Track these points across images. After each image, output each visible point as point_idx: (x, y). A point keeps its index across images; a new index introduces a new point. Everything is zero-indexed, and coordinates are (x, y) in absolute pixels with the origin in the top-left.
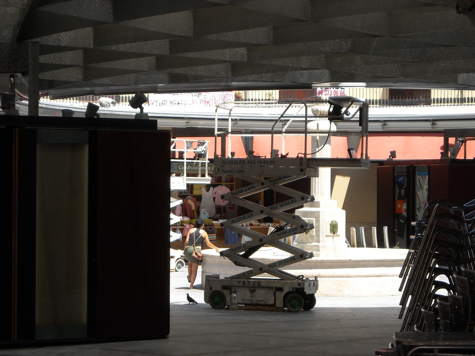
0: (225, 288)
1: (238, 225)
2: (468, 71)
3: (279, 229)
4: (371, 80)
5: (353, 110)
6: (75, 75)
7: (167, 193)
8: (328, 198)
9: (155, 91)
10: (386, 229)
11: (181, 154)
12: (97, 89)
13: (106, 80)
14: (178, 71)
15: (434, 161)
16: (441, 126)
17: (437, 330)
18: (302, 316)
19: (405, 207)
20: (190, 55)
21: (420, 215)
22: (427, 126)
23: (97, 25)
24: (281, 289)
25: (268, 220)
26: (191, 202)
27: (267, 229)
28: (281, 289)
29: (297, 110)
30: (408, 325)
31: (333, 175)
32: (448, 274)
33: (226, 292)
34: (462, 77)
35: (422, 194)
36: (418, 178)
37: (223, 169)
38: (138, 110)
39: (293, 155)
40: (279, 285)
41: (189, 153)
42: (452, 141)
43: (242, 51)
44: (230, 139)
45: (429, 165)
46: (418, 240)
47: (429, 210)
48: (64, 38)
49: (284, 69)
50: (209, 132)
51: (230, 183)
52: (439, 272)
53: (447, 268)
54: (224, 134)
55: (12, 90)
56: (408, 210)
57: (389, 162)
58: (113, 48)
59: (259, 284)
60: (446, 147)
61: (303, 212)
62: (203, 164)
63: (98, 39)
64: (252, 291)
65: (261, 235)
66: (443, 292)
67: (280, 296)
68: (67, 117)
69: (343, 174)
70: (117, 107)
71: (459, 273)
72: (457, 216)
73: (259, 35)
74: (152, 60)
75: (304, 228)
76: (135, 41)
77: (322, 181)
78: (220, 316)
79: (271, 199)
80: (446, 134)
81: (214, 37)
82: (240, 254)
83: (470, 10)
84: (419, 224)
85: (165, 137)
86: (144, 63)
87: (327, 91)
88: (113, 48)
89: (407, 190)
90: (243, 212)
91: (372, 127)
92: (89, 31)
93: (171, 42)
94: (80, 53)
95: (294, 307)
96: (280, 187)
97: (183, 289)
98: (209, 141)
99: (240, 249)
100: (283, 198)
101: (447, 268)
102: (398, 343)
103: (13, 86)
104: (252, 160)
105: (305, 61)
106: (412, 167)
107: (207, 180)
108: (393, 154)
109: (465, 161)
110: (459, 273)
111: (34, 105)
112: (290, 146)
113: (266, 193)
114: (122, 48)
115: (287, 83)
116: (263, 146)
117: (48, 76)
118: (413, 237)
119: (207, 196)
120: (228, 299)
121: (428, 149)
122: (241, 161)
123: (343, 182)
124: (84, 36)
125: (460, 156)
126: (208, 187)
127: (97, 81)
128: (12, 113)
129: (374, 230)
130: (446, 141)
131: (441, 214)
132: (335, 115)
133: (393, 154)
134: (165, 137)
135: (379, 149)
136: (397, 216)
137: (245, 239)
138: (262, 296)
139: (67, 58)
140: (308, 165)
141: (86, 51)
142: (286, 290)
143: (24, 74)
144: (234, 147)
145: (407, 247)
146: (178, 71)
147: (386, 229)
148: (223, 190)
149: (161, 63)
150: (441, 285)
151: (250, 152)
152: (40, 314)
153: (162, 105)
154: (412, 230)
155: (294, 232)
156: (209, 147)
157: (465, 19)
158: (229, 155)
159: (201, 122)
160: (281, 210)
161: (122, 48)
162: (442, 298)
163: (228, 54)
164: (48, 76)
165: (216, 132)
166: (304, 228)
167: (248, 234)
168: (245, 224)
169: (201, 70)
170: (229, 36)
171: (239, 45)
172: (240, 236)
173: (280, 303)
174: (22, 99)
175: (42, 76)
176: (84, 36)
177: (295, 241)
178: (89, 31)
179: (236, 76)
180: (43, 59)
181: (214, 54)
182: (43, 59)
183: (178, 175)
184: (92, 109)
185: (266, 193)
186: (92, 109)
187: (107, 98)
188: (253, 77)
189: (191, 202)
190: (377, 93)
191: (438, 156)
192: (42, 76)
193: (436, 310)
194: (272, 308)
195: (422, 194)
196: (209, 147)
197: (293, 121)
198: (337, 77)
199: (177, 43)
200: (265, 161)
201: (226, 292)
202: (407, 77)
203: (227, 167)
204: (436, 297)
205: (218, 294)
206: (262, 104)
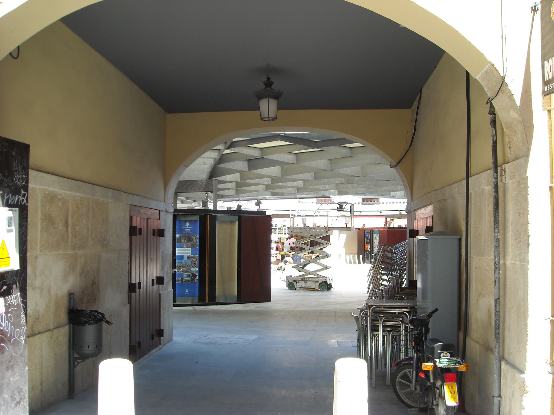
0: (294, 281)
1: (300, 255)
2: (395, 191)
3: (317, 256)
4: (356, 194)
5: (348, 207)
6: (232, 192)
7: (270, 242)
8: (338, 245)
9: (265, 199)
10: (361, 256)
11: (276, 225)
12: (241, 198)
13: (245, 195)
14: (274, 191)
15: (381, 228)
16: (384, 213)
17: (383, 298)
18: (326, 293)
19: (369, 247)
20: (280, 184)
21: (375, 250)
22: (378, 213)
23: (241, 172)
24: (318, 282)
25: (312, 252)
26: (280, 245)
27: (312, 256)
28: (318, 282)
29: (324, 206)
30: (370, 297)
31: (340, 233)
32: (387, 275)
33: (295, 283)
34: (392, 193)
35: (376, 242)
36: (374, 235)
37: (295, 233)
38: (258, 207)
39: (322, 226)
40: (317, 280)
41: (279, 225)
42: (388, 219)
43: (302, 182)
44: (296, 218)
45: (380, 231)
46: (375, 261)
47: (379, 249)
48: (228, 177)
49: (319, 190)
50: (288, 216)
51: (296, 237)
52: (383, 274)
53: (386, 272)
54: (294, 217)
55: (207, 199)
56: (370, 248)
57: (362, 228)
58: (248, 181)
59: (308, 280)
60: (386, 222)
61: (327, 250)
62: (285, 229)
63: (242, 178)
64: (306, 282)
65: (309, 259)
66: (385, 283)
67: (317, 284)
68: (229, 212)
69: (343, 233)
70: (249, 206)
71: (392, 275)
72: (391, 252)
73: (308, 176)
74: (264, 186)
75: (327, 256)
76: (257, 179)
77: (334, 236)
78: (292, 292)
79: (313, 244)
80: (386, 216)
81: (290, 177)
82: (302, 267)
83: (395, 166)
84: (375, 255)
85: (269, 218)
86: (261, 188)
87: (337, 199)
88: (248, 181)
89: (370, 240)
90: (302, 249)
91: (355, 214)
92: (238, 174)
93: (272, 179)
94: (235, 183)
95: (323, 289)
96: (317, 239)
97: (277, 282)
98: (287, 219)
99: (300, 265)
100: (318, 244)
101: (386, 272)
102: (367, 304)
103: (207, 197)
104: (306, 227)
105: (327, 187)
106: (372, 231)
107: (287, 236)
108: (364, 225)
109: (394, 228)
110: (392, 275)
111: (215, 205)
112: (322, 222)
113: (312, 241)
114: (252, 181)
115: (320, 196)
116: (310, 223)
117: (221, 193)
118: (372, 260)
119: (287, 243)
120: (295, 286)
121: (379, 223)
122: (301, 228)
123: (344, 236)
124: (236, 177)
125: (392, 226)
126: (287, 239)
127: (241, 195)
128: (207, 209)
129: (356, 256)
130: (386, 219)
131: (384, 251)
132: (340, 209)
133: (364, 225)
134: (269, 218)
135: (358, 223)
136: (365, 251)
137: (302, 261)
138: (311, 285)
139: (229, 185)
140: (329, 229)
141: (237, 183)
142: (319, 282)
143: (211, 192)
144: (298, 223)
145: (371, 264)
146: (274, 191)
147: (361, 256)
148: (293, 240)
149: (268, 187)
150: (384, 280)
151: (305, 225)
152: (218, 291)
153: (269, 206)
154: (372, 257)
155: (323, 258)
156: (287, 222)
157: (393, 170)
158: (295, 226)
159: (496, 385)
160: (317, 249)
161: (252, 181)
162: (386, 286)
163: (295, 184)
164: (221, 193)
165: (291, 216)
166: (327, 256)
167: (304, 259)
168: (302, 254)
169: (284, 190)
170: (296, 176)
171: (300, 180)
172: (300, 259)
173: (317, 288)
174: (210, 202)
175: (219, 193)
176: (236, 177)
177: (324, 261)
178: (238, 174)
179: (300, 192)
180: (219, 186)
181: (290, 184)
182: (219, 186)
183: (275, 234)
184: (239, 206)
185: (312, 241)
186: (239, 206)
187: (376, 205)
188: (306, 193)
189: (280, 245)
190: (359, 199)
191: (383, 226)
192: (219, 193)
193: (382, 291)
194: (314, 289)
195: (376, 242)
196: (287, 222)
197: (499, 239)
198: (341, 193)
199: (275, 180)
200: (311, 228)
201: (295, 283)
202: (370, 193)
203: (295, 231)
204: (382, 285)
205: (291, 285)
206: (309, 204)
